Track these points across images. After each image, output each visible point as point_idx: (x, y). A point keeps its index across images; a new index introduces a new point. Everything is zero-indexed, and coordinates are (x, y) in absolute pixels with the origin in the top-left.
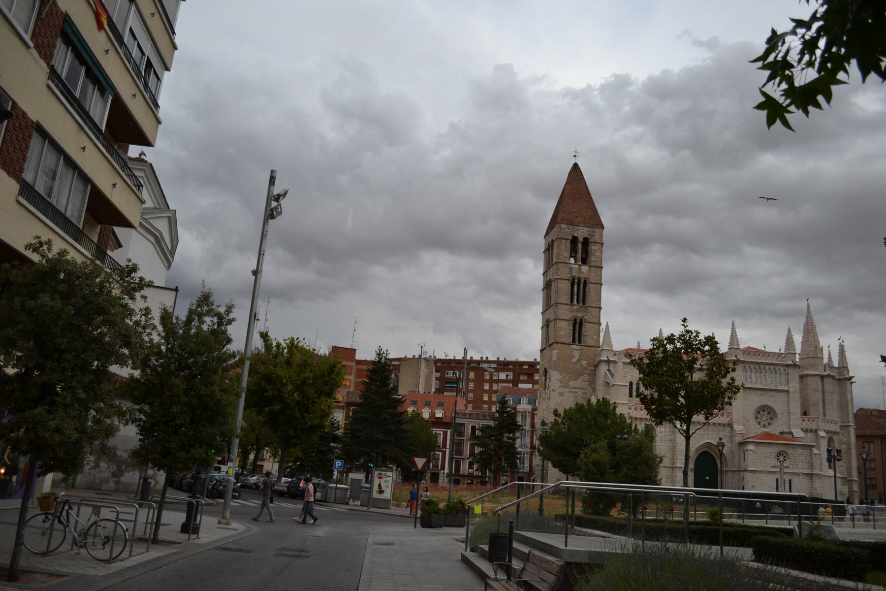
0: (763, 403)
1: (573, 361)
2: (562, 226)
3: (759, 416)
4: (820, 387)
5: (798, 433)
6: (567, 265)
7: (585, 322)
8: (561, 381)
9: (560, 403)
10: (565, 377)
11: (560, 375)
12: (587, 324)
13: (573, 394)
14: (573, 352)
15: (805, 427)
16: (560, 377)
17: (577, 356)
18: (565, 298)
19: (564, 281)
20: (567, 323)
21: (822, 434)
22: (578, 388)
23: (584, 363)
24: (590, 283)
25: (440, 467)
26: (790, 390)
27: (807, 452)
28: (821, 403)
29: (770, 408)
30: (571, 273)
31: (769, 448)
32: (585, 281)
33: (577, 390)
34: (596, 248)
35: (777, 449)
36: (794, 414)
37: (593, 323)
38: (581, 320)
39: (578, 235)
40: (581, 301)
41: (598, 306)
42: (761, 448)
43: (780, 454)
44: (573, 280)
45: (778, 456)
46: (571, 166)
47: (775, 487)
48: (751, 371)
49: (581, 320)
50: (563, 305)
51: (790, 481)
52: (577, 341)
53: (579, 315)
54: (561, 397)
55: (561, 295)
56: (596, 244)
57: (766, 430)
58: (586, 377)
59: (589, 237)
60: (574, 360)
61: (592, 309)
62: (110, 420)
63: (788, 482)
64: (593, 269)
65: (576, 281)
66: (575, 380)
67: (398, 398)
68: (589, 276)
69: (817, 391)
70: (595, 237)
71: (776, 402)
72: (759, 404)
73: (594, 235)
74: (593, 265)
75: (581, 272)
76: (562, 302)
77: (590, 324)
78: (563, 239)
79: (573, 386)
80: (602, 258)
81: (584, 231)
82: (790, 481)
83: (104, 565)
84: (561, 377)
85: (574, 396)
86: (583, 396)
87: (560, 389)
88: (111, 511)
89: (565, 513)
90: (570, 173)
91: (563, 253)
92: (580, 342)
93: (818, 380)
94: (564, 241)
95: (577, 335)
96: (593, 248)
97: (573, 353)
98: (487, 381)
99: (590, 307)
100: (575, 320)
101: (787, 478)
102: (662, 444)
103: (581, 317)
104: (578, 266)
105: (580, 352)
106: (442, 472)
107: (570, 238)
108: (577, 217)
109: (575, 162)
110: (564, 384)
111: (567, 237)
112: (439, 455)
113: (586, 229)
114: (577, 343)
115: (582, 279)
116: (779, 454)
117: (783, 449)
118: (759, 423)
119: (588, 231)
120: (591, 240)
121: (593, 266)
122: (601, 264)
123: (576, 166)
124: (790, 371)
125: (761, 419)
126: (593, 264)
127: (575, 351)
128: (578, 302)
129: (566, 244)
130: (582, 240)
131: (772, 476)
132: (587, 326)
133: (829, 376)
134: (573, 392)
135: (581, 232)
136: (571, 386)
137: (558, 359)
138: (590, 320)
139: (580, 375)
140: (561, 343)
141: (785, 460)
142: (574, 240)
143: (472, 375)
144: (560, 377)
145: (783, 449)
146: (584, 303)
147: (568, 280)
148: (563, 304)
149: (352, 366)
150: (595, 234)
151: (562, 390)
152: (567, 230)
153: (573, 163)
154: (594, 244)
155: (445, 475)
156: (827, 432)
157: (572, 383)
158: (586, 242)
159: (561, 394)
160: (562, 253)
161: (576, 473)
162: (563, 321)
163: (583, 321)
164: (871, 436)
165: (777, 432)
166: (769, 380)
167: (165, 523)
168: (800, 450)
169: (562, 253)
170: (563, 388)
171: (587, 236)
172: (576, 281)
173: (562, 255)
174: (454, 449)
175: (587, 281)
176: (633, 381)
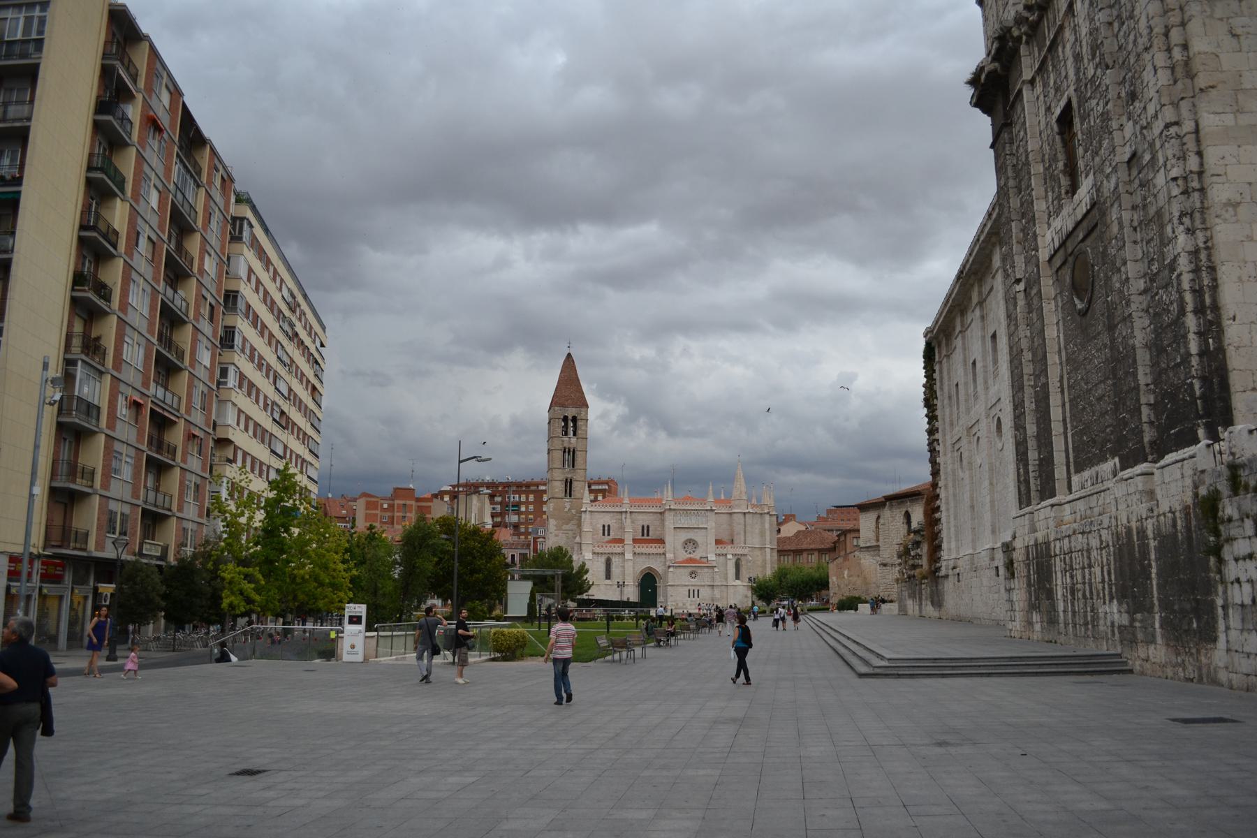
0: (689, 537)
4: (742, 522)
5: (712, 557)
8: (556, 526)
15: (718, 552)
17: (568, 507)
18: (558, 464)
21: (729, 556)
23: (573, 511)
27: (710, 570)
28: (742, 533)
29: (687, 540)
35: (690, 570)
53: (569, 476)
57: (691, 556)
58: (574, 522)
60: (566, 510)
64: (580, 440)
69: (740, 524)
71: (698, 537)
92: (570, 496)
93: (741, 516)
96: (579, 423)
110: (559, 528)
113: (574, 409)
116: (692, 573)
117: (694, 569)
123: (569, 355)
124: (709, 513)
126: (580, 436)
133: (749, 512)
135: (571, 412)
142: (565, 419)
143: (531, 498)
145: (694, 569)
146: (573, 467)
149: (349, 623)
151: (556, 532)
157: (565, 527)
158: (574, 419)
159: (556, 535)
161: (1204, 530)
164: (812, 550)
165: (698, 558)
167: (978, 379)
168: (706, 570)
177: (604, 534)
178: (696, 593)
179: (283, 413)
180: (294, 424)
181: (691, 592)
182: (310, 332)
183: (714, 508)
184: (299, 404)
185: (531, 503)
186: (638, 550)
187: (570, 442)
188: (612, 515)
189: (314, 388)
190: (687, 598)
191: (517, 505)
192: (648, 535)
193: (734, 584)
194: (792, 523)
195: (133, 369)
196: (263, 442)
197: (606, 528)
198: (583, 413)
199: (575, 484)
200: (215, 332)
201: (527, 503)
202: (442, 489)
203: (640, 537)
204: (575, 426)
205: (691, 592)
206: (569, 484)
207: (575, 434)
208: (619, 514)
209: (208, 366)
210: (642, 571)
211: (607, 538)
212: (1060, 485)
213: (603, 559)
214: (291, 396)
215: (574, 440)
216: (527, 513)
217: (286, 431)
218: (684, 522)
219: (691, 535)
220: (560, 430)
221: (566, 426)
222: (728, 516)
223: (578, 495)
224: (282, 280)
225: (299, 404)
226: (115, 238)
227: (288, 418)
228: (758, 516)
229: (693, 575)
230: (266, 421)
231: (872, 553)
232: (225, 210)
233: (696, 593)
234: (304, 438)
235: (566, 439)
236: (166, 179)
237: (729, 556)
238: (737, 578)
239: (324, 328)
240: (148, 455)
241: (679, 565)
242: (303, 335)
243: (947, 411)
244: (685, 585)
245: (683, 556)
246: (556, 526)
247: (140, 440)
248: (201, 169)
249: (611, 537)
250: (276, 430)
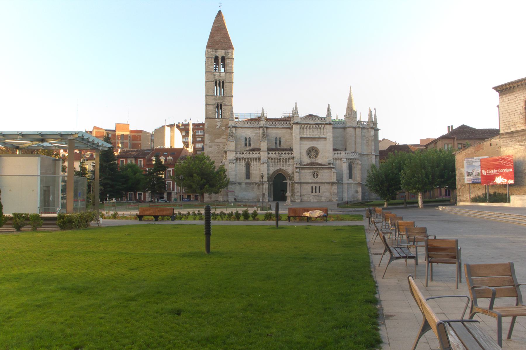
1: (217, 128)
2: (209, 51)
3: (309, 152)
6: (213, 73)
7: (223, 105)
8: (210, 139)
9: (210, 151)
10: (212, 137)
11: (210, 136)
12: (225, 106)
13: (217, 146)
14: (216, 123)
16: (209, 137)
19: (211, 82)
20: (213, 106)
22: (220, 143)
24: (226, 82)
25: (172, 189)
26: (327, 137)
30: (214, 78)
31: (308, 170)
32: (223, 82)
33: (219, 144)
37: (228, 105)
38: (221, 104)
39: (218, 55)
41: (231, 95)
42: (304, 170)
43: (315, 173)
44: (216, 81)
45: (313, 174)
46: (217, 12)
47: (311, 191)
49: (221, 104)
50: (210, 97)
53: (220, 101)
54: (210, 148)
55: (209, 91)
56: (230, 59)
57: (313, 160)
59: (225, 56)
60: (218, 127)
61: (227, 97)
63: (318, 188)
65: (218, 82)
66: (218, 138)
68: (225, 79)
70: (229, 55)
72: (309, 146)
73: (228, 54)
74: (228, 72)
75: (221, 76)
76: (210, 95)
77: (226, 106)
78: (209, 58)
79: (217, 142)
80: (232, 67)
81: (222, 52)
83: (375, 278)
84: (210, 137)
85: (218, 147)
86: (223, 146)
87: (210, 144)
89: (227, 209)
90: (216, 17)
91: (210, 66)
94: (210, 59)
96: (227, 61)
97: (217, 123)
99: (226, 96)
100: (218, 104)
101: (318, 186)
102: (254, 171)
103: (221, 102)
104: (218, 73)
105: (221, 122)
106: (173, 192)
107: (214, 57)
109: (219, 10)
111: (211, 57)
112: (171, 182)
113: (223, 51)
115: (221, 81)
118: (310, 157)
119: (224, 52)
120: (226, 57)
121: (228, 73)
122: (232, 71)
123: (220, 12)
125: (311, 154)
127: (218, 122)
129: (211, 61)
130: (221, 58)
131: (310, 185)
132: (225, 107)
134: (217, 145)
135: (220, 53)
136: (216, 142)
137: (208, 128)
138: (226, 104)
139: (221, 135)
140: (210, 118)
141: (317, 174)
144: (209, 137)
147: (213, 82)
148: (211, 96)
150: (229, 53)
151: (211, 144)
152: (211, 52)
153: (218, 11)
154: (228, 59)
155: (175, 194)
157: (217, 140)
158: (223, 59)
159: (210, 147)
160: (209, 66)
162: (210, 106)
163: (222, 105)
169: (209, 66)
170: (212, 143)
171: (224, 55)
172: (218, 82)
173: (209, 67)
175: (224, 82)
176: (247, 137)
178: (318, 189)
181: (314, 188)
186: (270, 155)
188: (252, 130)
198: (230, 54)
205: (314, 188)
208: (258, 129)
211: (248, 148)
212: (460, 142)
213: (243, 163)
218: (307, 133)
219: (314, 144)
222: (343, 130)
229: (315, 175)
231: (519, 138)
233: (318, 189)
241: (302, 167)
243: (266, 187)
244: (309, 183)
245: (306, 160)
246: (210, 139)
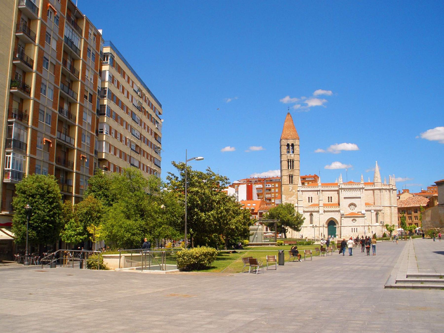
17: (291, 189)
20: (287, 176)
21: (372, 211)
30: (287, 158)
34: (296, 147)
36: (363, 205)
40: (292, 168)
44: (288, 160)
48: (347, 191)
51: (357, 228)
52: (291, 183)
53: (291, 173)
57: (353, 211)
60: (290, 190)
62: (101, 226)
65: (289, 160)
67: (323, 89)
82: (357, 228)
88: (382, 192)
92: (292, 183)
95: (291, 181)
98: (277, 188)
107: (286, 144)
108: (289, 136)
114: (291, 184)
118: (350, 209)
128: (291, 169)
146: (293, 168)
156: (375, 210)
158: (293, 145)
166: (354, 194)
174: (147, 254)
177: (309, 202)
178: (356, 230)
179: (137, 146)
180: (144, 151)
181: (353, 229)
182: (152, 107)
183: (363, 187)
184: (148, 142)
185: (277, 188)
187: (291, 157)
189: (156, 134)
190: (351, 232)
191: (270, 190)
192: (331, 201)
193: (375, 225)
194: (406, 194)
195: (86, 132)
196: (126, 160)
197: (310, 199)
199: (294, 177)
200: (93, 107)
201: (275, 188)
202: (234, 183)
203: (327, 203)
204: (293, 148)
205: (353, 229)
206: (291, 177)
207: (293, 152)
209: (90, 123)
210: (328, 220)
211: (310, 204)
214: (141, 138)
215: (292, 156)
216: (275, 193)
217: (140, 155)
220: (286, 151)
221: (289, 148)
223: (296, 183)
224: (133, 82)
225: (148, 142)
226: (32, 63)
227: (140, 148)
228: (388, 191)
230: (127, 150)
232: (96, 49)
233: (356, 230)
234: (151, 159)
235: (289, 155)
236: (60, 35)
237: (372, 211)
238: (377, 222)
239: (160, 106)
240: (56, 166)
242: (148, 109)
247: (51, 158)
248: (82, 30)
249: (313, 203)
250: (134, 155)
